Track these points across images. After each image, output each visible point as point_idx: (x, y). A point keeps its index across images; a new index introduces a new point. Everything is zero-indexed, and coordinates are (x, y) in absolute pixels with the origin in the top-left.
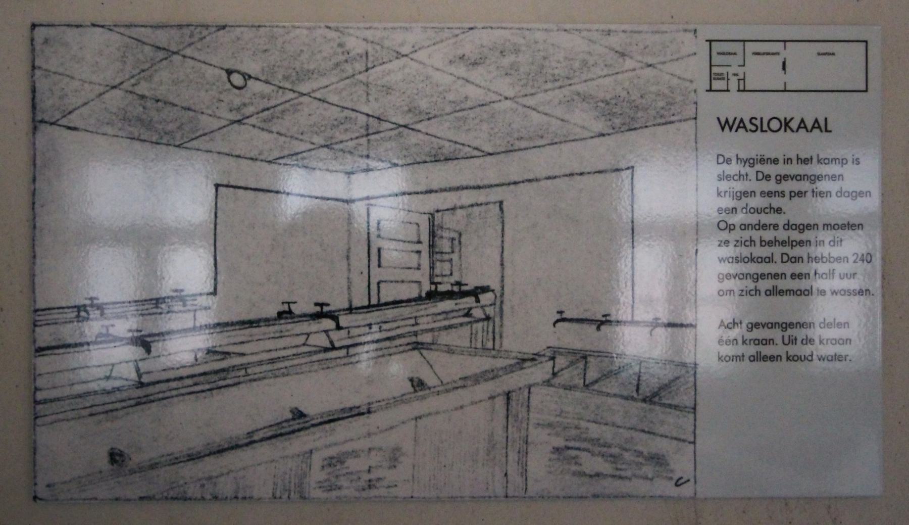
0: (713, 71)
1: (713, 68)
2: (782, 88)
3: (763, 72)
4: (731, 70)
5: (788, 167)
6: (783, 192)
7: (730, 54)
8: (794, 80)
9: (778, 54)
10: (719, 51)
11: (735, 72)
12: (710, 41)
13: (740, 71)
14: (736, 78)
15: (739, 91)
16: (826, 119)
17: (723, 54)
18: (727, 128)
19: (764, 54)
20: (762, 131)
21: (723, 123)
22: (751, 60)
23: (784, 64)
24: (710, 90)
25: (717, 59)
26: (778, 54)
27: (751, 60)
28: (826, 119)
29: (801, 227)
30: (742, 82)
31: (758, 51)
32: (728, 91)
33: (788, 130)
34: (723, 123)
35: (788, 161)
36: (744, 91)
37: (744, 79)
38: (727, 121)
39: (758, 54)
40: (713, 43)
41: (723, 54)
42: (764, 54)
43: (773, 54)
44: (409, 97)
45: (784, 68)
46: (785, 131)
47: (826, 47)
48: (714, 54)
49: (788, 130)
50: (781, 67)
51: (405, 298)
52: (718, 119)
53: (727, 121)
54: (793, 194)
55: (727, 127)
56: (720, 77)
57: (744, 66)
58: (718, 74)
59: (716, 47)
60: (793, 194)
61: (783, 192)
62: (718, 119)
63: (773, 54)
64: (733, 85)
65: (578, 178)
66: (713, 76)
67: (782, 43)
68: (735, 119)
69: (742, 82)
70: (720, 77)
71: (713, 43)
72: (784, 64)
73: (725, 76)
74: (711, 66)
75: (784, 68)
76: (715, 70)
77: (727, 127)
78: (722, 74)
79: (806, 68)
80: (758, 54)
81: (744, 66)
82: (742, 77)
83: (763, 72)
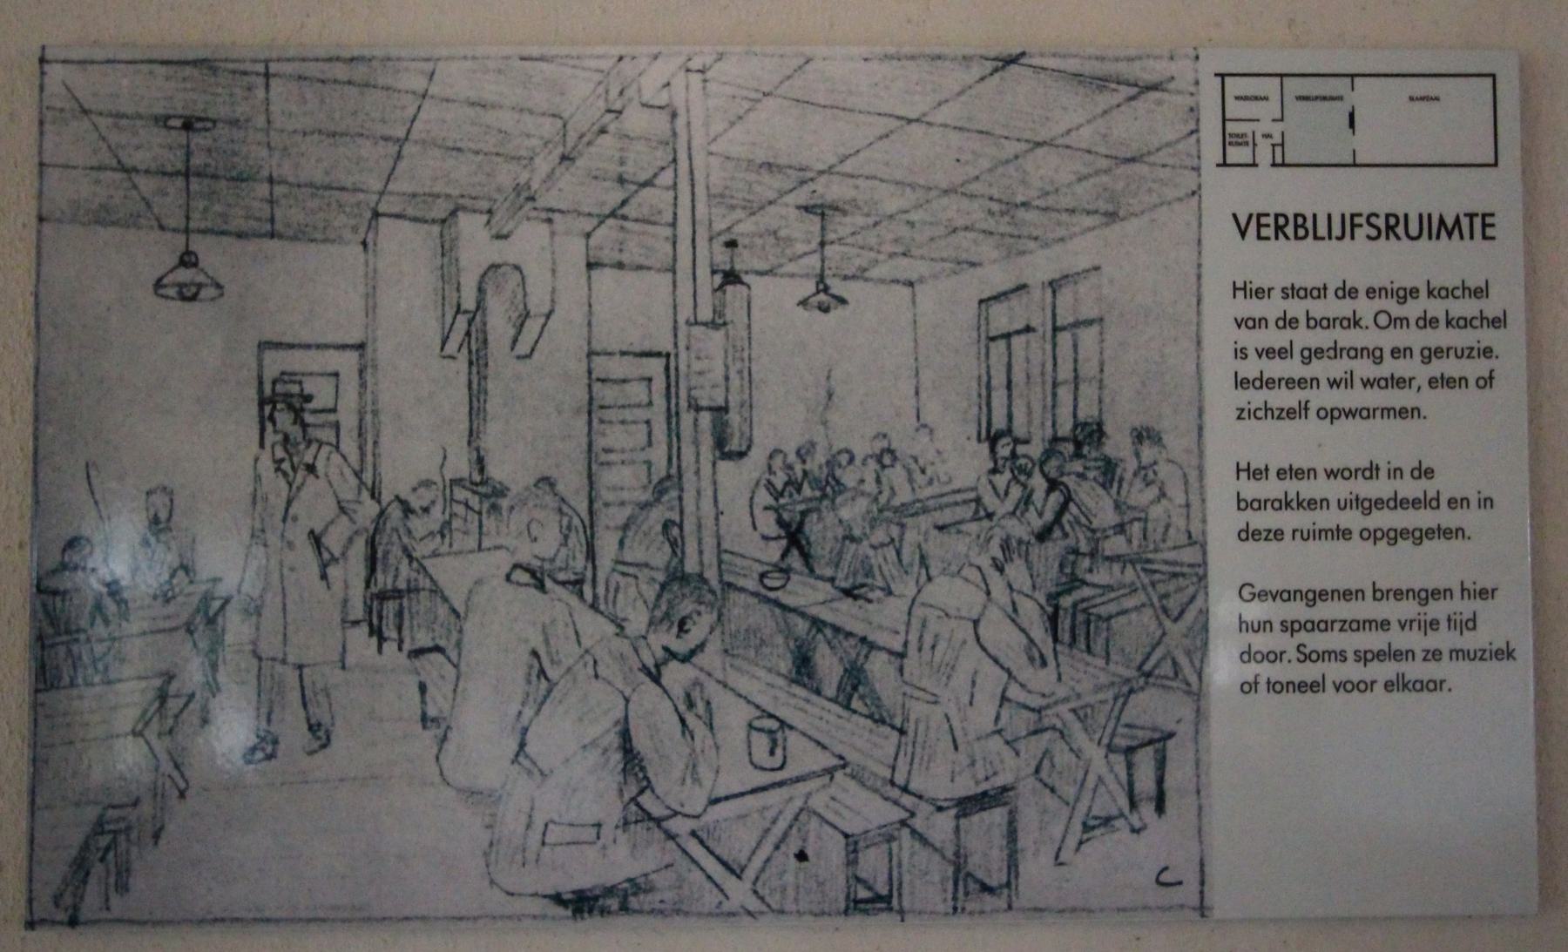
1: (1228, 124)
3: (1314, 130)
4: (1261, 128)
5: (1432, 665)
6: (1343, 652)
7: (1256, 98)
8: (1368, 144)
9: (1340, 98)
10: (1238, 94)
11: (1266, 131)
12: (1222, 76)
13: (1276, 130)
14: (1270, 141)
15: (1274, 165)
17: (1246, 98)
18: (1450, 222)
21: (1456, 232)
22: (1293, 107)
23: (1352, 116)
24: (1224, 164)
25: (1233, 109)
26: (1340, 98)
27: (1294, 109)
29: (1392, 534)
30: (1278, 150)
31: (1305, 93)
32: (1254, 165)
33: (1391, 235)
34: (1456, 232)
35: (1396, 473)
36: (1283, 165)
38: (1450, 235)
39: (1306, 98)
40: (1227, 79)
41: (1246, 98)
45: (1352, 124)
48: (1230, 101)
49: (1391, 235)
50: (1347, 122)
52: (1235, 216)
53: (1450, 235)
55: (1450, 226)
56: (1240, 140)
59: (1234, 86)
61: (1343, 652)
62: (1235, 216)
64: (1264, 154)
66: (1228, 139)
67: (1348, 80)
68: (1251, 216)
69: (1278, 150)
70: (1240, 140)
72: (1352, 116)
74: (1224, 120)
75: (1352, 124)
76: (1232, 128)
77: (1450, 226)
78: (1243, 135)
80: (1306, 98)
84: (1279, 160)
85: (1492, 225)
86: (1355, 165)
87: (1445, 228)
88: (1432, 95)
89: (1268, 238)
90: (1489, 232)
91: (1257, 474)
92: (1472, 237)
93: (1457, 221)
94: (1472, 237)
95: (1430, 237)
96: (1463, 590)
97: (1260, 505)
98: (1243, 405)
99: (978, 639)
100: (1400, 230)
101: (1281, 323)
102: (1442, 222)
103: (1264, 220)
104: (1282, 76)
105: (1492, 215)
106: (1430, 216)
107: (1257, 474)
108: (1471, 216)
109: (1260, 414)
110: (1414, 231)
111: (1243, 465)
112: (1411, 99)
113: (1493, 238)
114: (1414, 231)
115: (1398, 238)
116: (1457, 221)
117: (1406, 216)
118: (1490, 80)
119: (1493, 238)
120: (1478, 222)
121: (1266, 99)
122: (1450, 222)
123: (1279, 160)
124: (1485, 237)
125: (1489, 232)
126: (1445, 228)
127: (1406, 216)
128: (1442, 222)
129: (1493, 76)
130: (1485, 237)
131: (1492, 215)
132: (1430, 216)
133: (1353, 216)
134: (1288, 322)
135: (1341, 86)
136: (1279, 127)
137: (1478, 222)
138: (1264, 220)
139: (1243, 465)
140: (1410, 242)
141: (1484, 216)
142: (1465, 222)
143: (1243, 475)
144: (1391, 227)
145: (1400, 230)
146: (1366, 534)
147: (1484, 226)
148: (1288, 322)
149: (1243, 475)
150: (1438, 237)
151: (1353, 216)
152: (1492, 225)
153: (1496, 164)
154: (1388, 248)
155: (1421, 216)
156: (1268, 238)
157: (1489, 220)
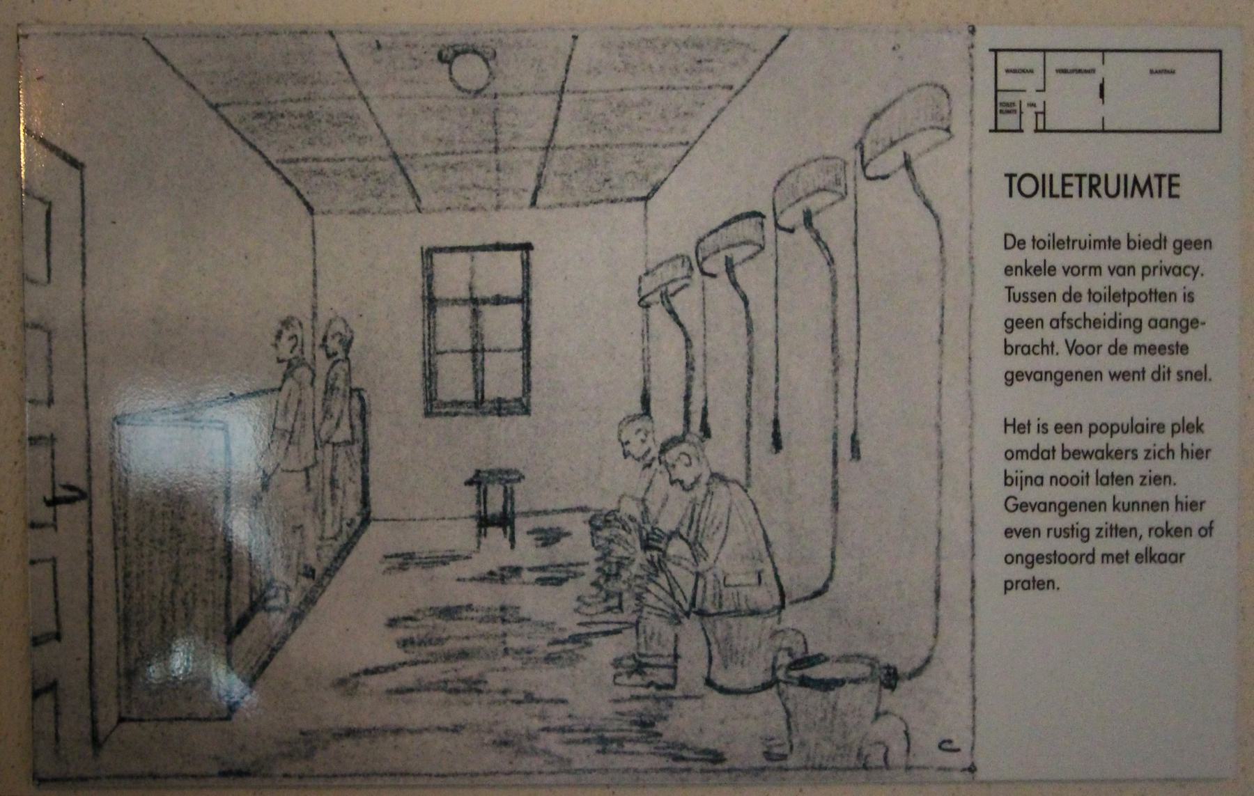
0: (999, 100)
2: (1107, 55)
3: (1071, 101)
9: (1093, 71)
12: (996, 51)
13: (1038, 99)
14: (1034, 109)
15: (1037, 131)
16: (1011, 195)
18: (1142, 182)
19: (1073, 71)
20: (1052, 195)
21: (1147, 191)
22: (1051, 73)
24: (996, 130)
26: (1093, 71)
28: (1011, 195)
30: (1041, 117)
32: (1021, 131)
34: (1147, 191)
36: (1044, 130)
37: (1044, 113)
38: (1142, 193)
39: (1064, 71)
41: (1015, 71)
42: (1073, 71)
43: (1086, 71)
44: (320, 121)
45: (1102, 95)
46: (1091, 196)
47: (1162, 58)
48: (1001, 71)
51: (745, 349)
53: (1142, 193)
54: (1093, 428)
55: (1142, 185)
56: (1009, 108)
57: (1044, 90)
58: (1007, 105)
59: (1005, 60)
60: (1093, 428)
63: (1086, 71)
64: (1029, 121)
65: (707, 293)
66: (999, 108)
69: (1041, 117)
70: (1009, 108)
71: (1000, 55)
73: (1017, 108)
74: (996, 91)
75: (1102, 95)
76: (1003, 97)
77: (1142, 185)
79: (1135, 93)
80: (1064, 71)
81: (1044, 90)
82: (1040, 109)
83: (1071, 101)
84: (1041, 126)
85: (1178, 185)
86: (1103, 131)
87: (1137, 187)
88: (1169, 68)
89: (1071, 196)
90: (1175, 190)
91: (1021, 428)
92: (1160, 195)
93: (1148, 182)
94: (1160, 195)
95: (1126, 195)
96: (1177, 503)
97: (1021, 454)
98: (1150, 446)
99: (688, 340)
100: (1101, 189)
101: (1067, 297)
102: (1136, 181)
103: (1068, 180)
104: (1044, 51)
105: (1177, 176)
106: (1126, 177)
107: (1021, 428)
108: (1160, 177)
109: (1164, 454)
110: (1112, 190)
111: (1010, 421)
112: (1151, 72)
113: (1177, 196)
114: (1112, 190)
115: (1099, 196)
116: (1148, 182)
117: (1106, 176)
118: (1217, 55)
119: (1177, 196)
120: (1165, 181)
121: (1031, 71)
122: (1142, 182)
123: (1041, 126)
124: (1171, 196)
125: (1175, 190)
126: (1137, 187)
127: (1106, 176)
128: (1136, 181)
129: (1220, 52)
130: (1171, 196)
131: (1177, 176)
132: (1126, 177)
133: (1064, 176)
134: (1072, 296)
135: (1093, 60)
136: (1042, 96)
137: (1165, 181)
138: (1068, 180)
139: (1010, 421)
140: (1112, 200)
141: (1171, 176)
142: (1155, 182)
143: (1010, 429)
144: (1094, 185)
145: (1101, 189)
146: (1039, 481)
147: (1171, 185)
148: (1072, 296)
149: (1010, 429)
150: (1132, 195)
151: (1064, 176)
152: (1178, 185)
153: (1220, 131)
154: (1100, 204)
155: (1118, 177)
156: (1071, 196)
157: (1174, 180)
